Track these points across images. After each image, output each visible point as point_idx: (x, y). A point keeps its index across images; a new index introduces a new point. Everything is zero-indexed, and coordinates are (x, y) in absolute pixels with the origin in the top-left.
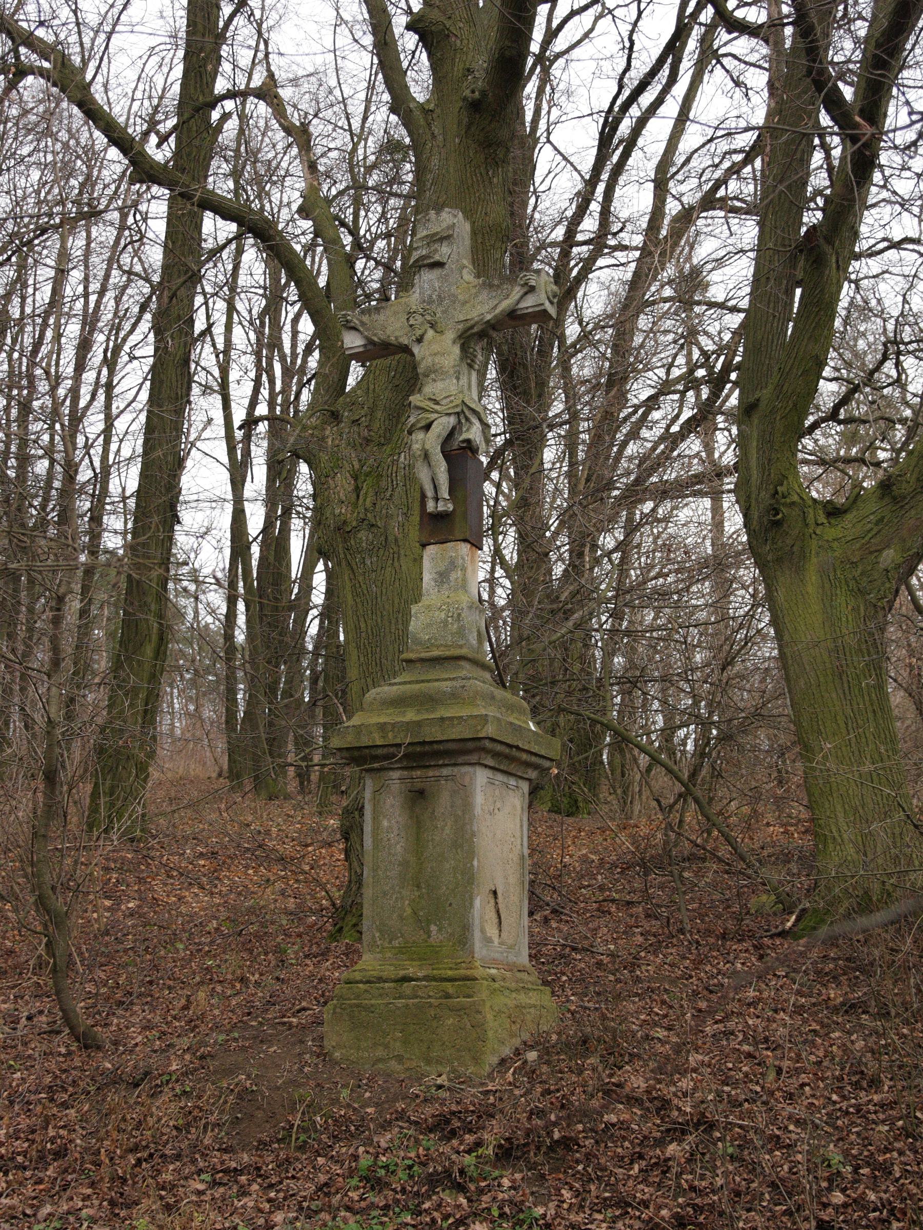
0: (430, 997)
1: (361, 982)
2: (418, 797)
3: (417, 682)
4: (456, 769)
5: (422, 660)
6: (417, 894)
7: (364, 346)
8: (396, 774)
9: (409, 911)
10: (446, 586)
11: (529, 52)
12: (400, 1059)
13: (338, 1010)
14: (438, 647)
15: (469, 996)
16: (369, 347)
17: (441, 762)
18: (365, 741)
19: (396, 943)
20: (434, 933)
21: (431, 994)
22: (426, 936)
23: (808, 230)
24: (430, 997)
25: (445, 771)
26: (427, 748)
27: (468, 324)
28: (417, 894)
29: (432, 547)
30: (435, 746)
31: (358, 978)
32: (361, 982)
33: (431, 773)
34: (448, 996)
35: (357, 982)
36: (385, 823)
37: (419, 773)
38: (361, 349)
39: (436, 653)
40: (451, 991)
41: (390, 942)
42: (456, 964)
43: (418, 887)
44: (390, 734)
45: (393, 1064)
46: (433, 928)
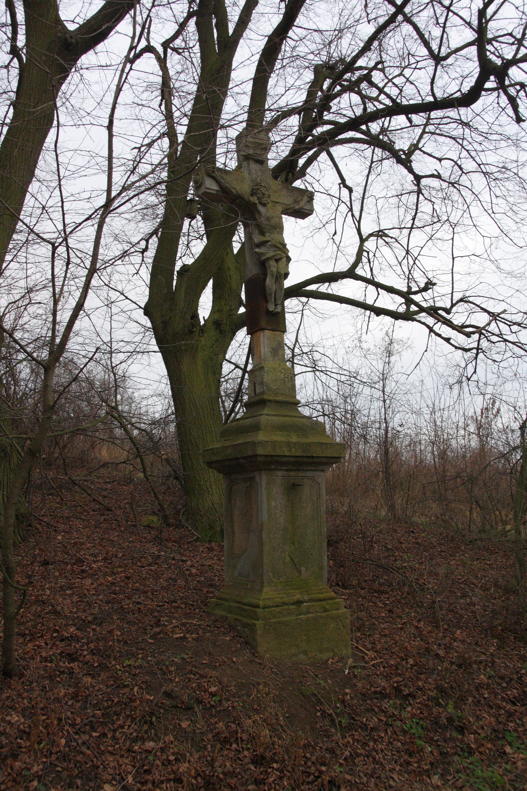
0: (317, 612)
1: (273, 606)
2: (293, 488)
3: (276, 415)
4: (314, 473)
5: (277, 402)
6: (293, 548)
7: (217, 191)
8: (280, 473)
9: (288, 559)
10: (276, 357)
11: (430, 111)
12: (305, 653)
13: (267, 627)
14: (282, 395)
15: (337, 609)
16: (219, 193)
17: (309, 468)
18: (278, 452)
19: (282, 579)
20: (303, 571)
21: (317, 610)
22: (298, 574)
23: (52, 124)
24: (317, 612)
25: (309, 474)
26: (311, 460)
27: (288, 207)
28: (293, 548)
29: (267, 331)
30: (315, 459)
31: (271, 604)
32: (273, 606)
33: (300, 474)
34: (326, 610)
35: (270, 607)
36: (273, 504)
37: (293, 473)
38: (214, 192)
39: (280, 398)
40: (328, 607)
41: (279, 579)
42: (320, 590)
43: (293, 543)
44: (293, 450)
45: (302, 657)
46: (303, 569)
